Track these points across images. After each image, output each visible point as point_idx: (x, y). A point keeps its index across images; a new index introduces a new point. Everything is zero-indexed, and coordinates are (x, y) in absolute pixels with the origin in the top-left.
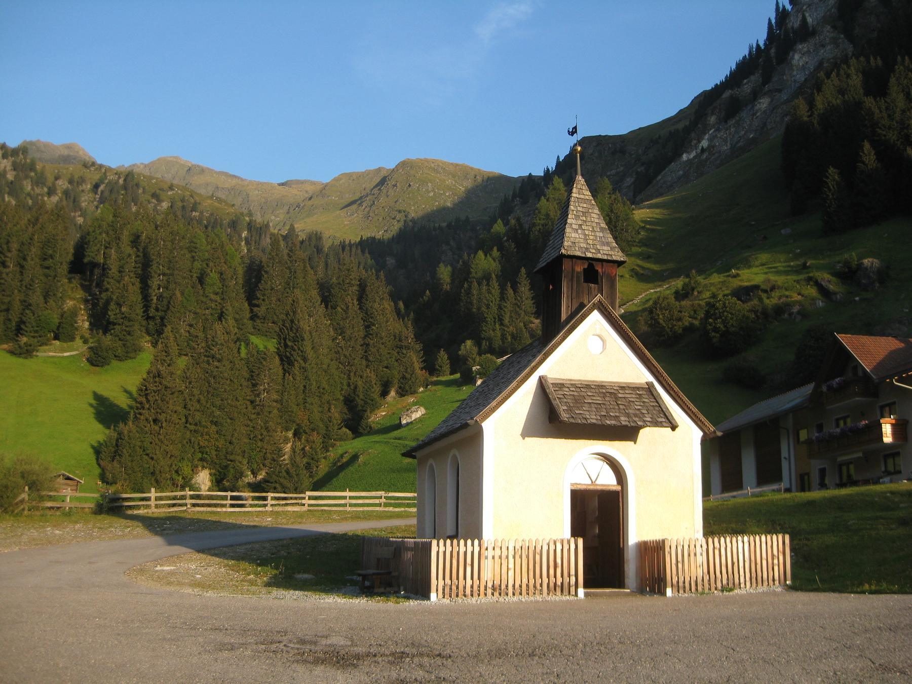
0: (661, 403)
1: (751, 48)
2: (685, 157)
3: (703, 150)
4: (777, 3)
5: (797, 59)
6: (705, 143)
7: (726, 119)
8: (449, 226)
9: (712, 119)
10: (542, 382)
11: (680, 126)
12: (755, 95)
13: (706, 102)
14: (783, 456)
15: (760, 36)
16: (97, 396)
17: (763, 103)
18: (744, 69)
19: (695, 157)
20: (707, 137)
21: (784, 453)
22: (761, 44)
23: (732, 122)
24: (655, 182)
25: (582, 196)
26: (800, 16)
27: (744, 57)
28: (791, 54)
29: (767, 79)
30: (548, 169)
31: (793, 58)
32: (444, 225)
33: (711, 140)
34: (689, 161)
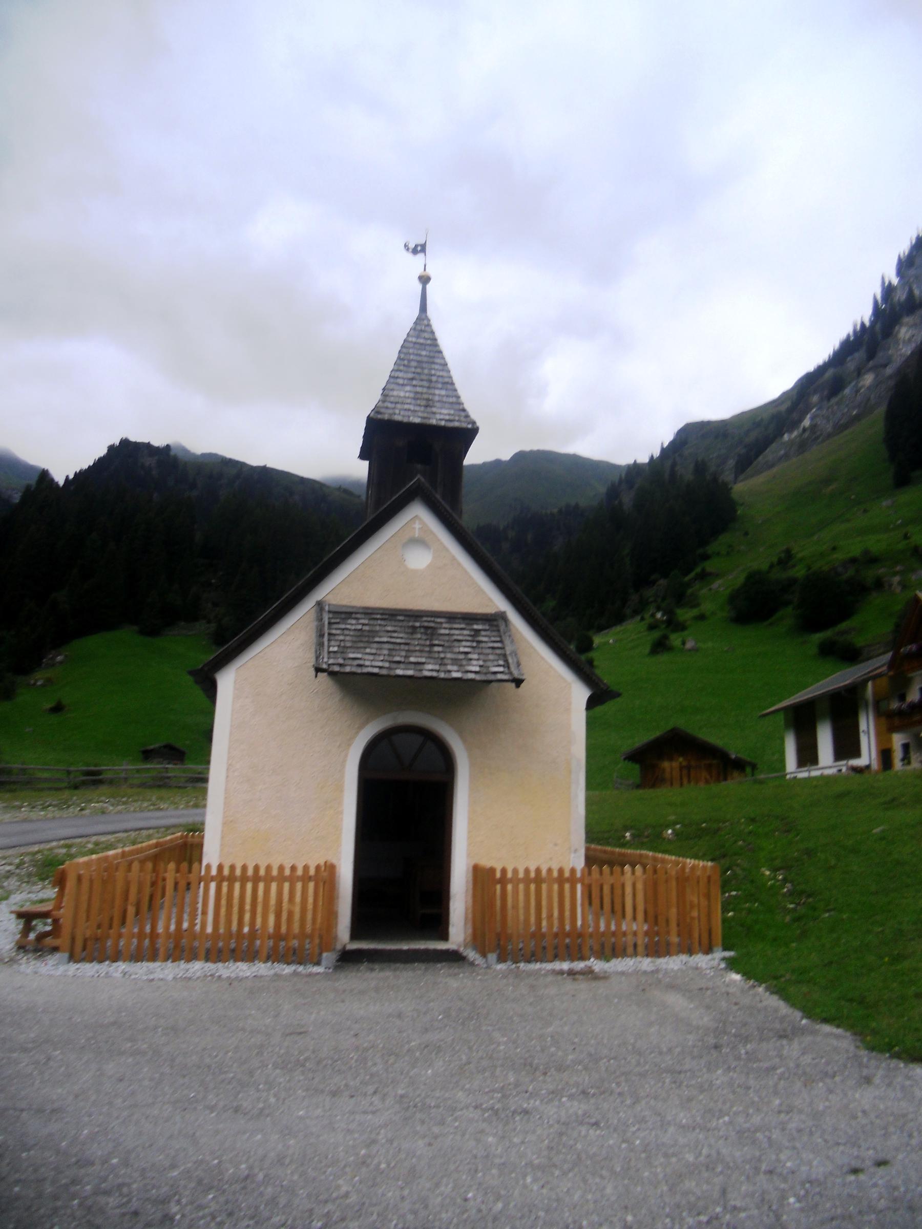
0: (344, 610)
1: (855, 326)
2: (786, 437)
3: (805, 430)
4: (883, 279)
5: (903, 332)
6: (807, 423)
7: (829, 398)
8: (560, 511)
9: (815, 399)
10: (320, 605)
11: (783, 408)
12: (859, 373)
13: (809, 385)
14: (861, 730)
15: (865, 313)
16: (618, 695)
17: (868, 379)
18: (847, 349)
19: (796, 437)
20: (809, 416)
21: (863, 726)
22: (867, 324)
23: (834, 400)
24: (755, 463)
25: (422, 341)
26: (907, 289)
27: (848, 336)
28: (897, 328)
29: (871, 355)
30: (652, 456)
31: (899, 332)
32: (555, 511)
33: (812, 419)
34: (792, 442)
